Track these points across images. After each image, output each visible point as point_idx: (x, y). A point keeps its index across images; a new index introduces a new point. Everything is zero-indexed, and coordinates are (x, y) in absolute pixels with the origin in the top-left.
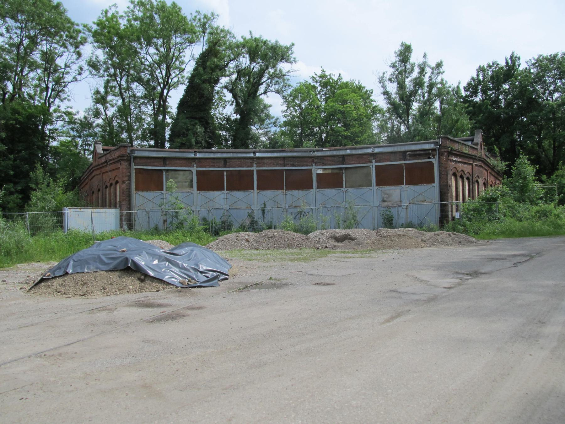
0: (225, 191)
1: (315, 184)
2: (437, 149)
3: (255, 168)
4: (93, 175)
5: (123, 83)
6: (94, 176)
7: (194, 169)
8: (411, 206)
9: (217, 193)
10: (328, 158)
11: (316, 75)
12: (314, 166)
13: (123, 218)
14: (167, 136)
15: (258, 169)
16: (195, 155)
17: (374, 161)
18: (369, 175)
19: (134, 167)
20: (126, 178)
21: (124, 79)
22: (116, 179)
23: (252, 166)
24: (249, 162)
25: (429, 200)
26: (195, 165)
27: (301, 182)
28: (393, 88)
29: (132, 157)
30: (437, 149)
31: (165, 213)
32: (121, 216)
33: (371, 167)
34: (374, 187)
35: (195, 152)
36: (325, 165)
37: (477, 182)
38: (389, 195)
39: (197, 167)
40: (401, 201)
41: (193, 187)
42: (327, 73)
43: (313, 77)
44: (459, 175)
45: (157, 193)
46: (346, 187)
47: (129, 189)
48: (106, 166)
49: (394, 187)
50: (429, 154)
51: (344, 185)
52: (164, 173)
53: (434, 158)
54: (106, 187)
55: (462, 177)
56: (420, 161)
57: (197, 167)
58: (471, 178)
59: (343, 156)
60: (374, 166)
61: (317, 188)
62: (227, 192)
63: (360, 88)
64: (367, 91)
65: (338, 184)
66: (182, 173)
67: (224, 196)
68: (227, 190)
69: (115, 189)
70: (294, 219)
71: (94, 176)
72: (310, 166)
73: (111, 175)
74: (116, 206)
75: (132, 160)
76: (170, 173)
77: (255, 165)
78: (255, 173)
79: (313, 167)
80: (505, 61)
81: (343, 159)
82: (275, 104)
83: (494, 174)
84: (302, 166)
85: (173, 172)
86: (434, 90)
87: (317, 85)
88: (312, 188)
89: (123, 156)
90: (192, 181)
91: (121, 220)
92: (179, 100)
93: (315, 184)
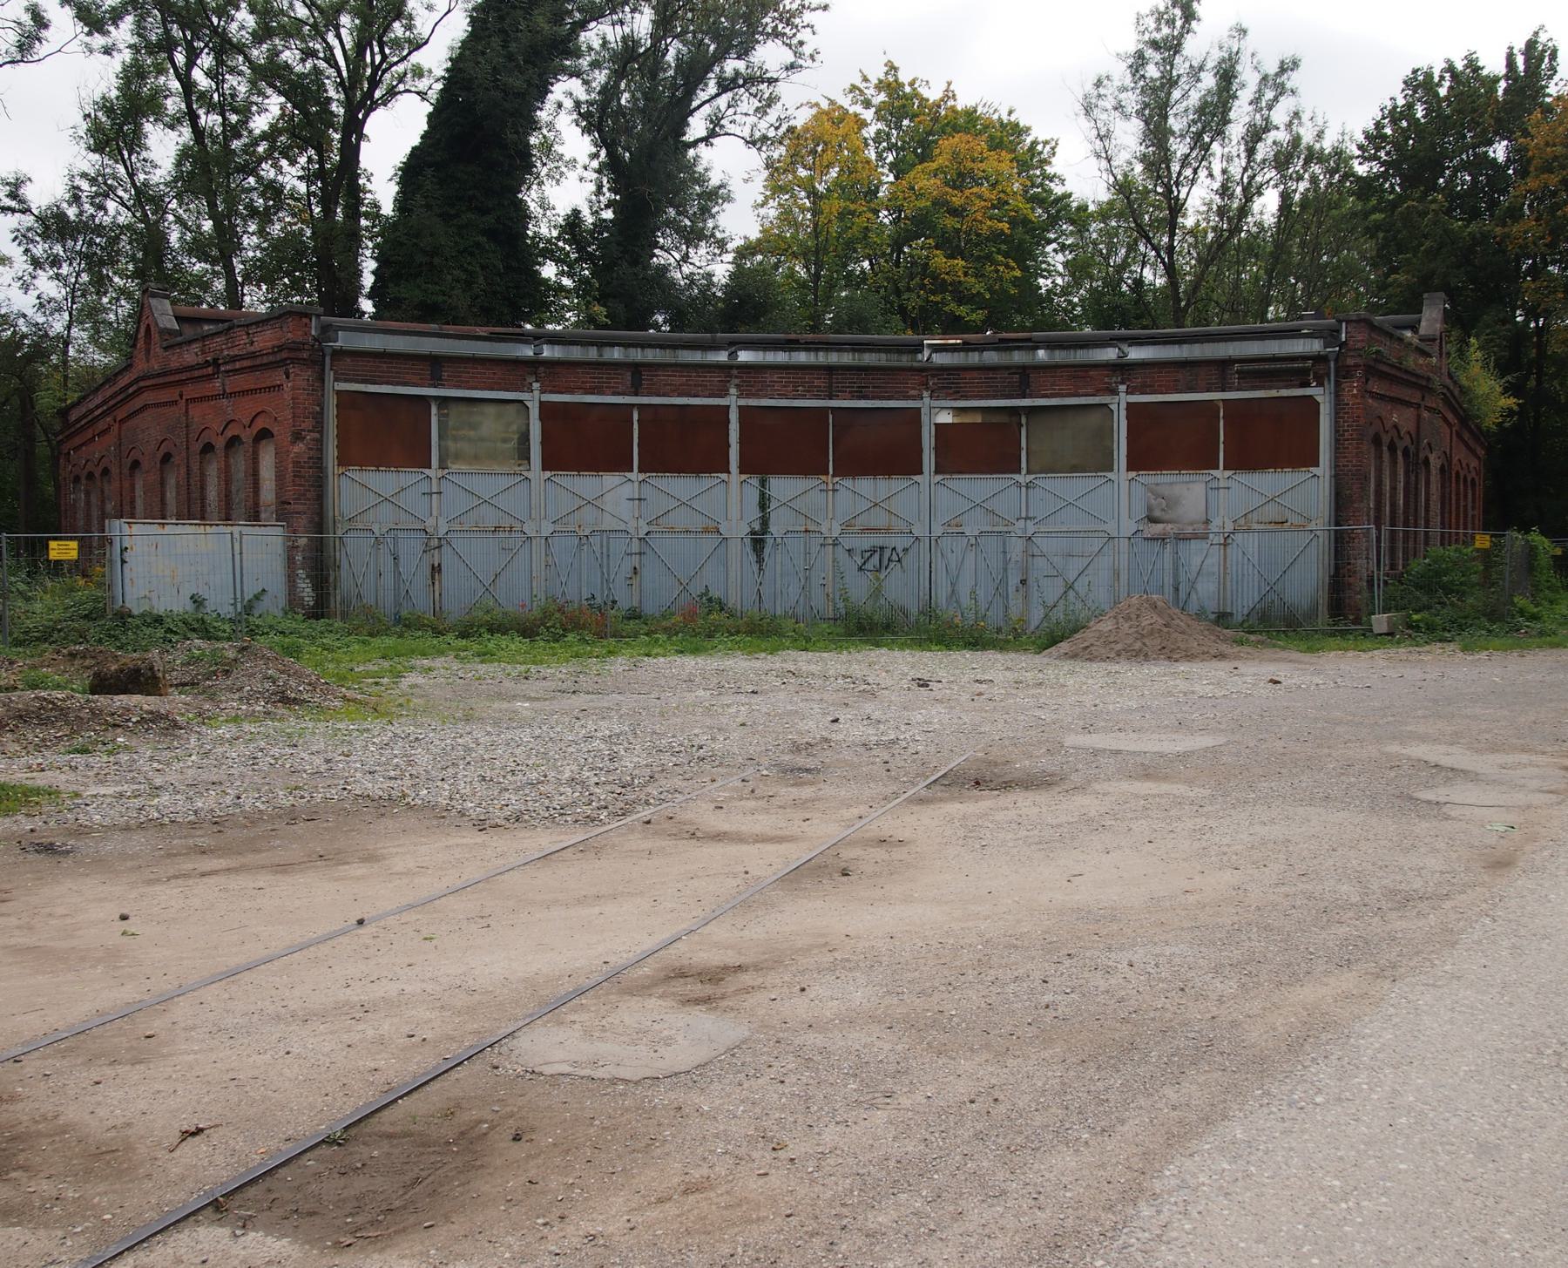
0: (635, 475)
1: (928, 459)
2: (1332, 357)
3: (733, 401)
4: (137, 403)
5: (198, 75)
6: (145, 407)
7: (533, 399)
8: (1238, 537)
9: (610, 480)
10: (975, 374)
11: (866, 80)
12: (927, 400)
13: (299, 558)
14: (368, 280)
15: (743, 402)
16: (733, 355)
17: (1123, 388)
18: (1105, 434)
19: (337, 385)
20: (308, 424)
21: (206, 60)
22: (260, 423)
23: (723, 393)
24: (716, 378)
25: (1297, 520)
26: (536, 385)
27: (889, 452)
28: (1129, 137)
29: (328, 351)
30: (1332, 357)
31: (435, 543)
32: (291, 550)
33: (1114, 407)
34: (1120, 471)
35: (732, 343)
36: (966, 397)
37: (1427, 462)
38: (1171, 503)
39: (543, 392)
40: (1207, 522)
41: (528, 459)
42: (904, 77)
43: (854, 88)
44: (1386, 439)
45: (408, 477)
46: (1029, 472)
47: (318, 463)
48: (209, 377)
49: (1186, 476)
50: (1305, 372)
51: (1024, 465)
52: (434, 410)
53: (1320, 384)
54: (208, 448)
55: (1392, 448)
56: (1273, 393)
57: (543, 392)
58: (1412, 449)
59: (1024, 370)
60: (1123, 406)
61: (937, 472)
62: (642, 476)
63: (1018, 130)
64: (1035, 143)
65: (1006, 463)
66: (491, 410)
67: (629, 490)
68: (640, 471)
69: (255, 461)
70: (860, 569)
71: (145, 407)
72: (913, 398)
73: (244, 409)
74: (254, 516)
75: (328, 359)
76: (454, 410)
77: (733, 391)
78: (734, 416)
79: (925, 403)
80: (1504, 63)
81: (1024, 380)
82: (738, 180)
83: (1466, 436)
84: (889, 398)
85: (463, 408)
86: (1263, 150)
87: (868, 115)
88: (921, 473)
89: (295, 347)
90: (525, 438)
91: (290, 561)
92: (408, 150)
93: (928, 459)
